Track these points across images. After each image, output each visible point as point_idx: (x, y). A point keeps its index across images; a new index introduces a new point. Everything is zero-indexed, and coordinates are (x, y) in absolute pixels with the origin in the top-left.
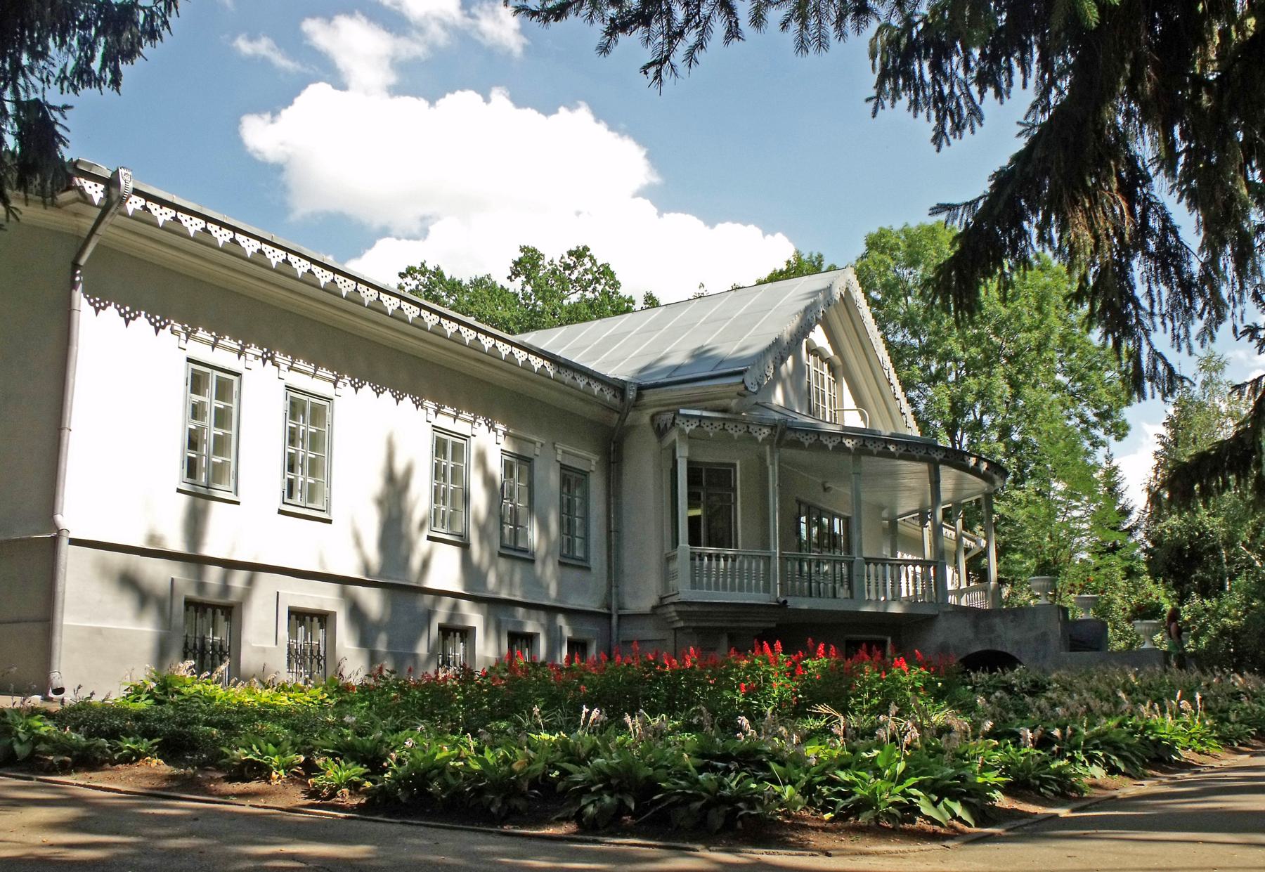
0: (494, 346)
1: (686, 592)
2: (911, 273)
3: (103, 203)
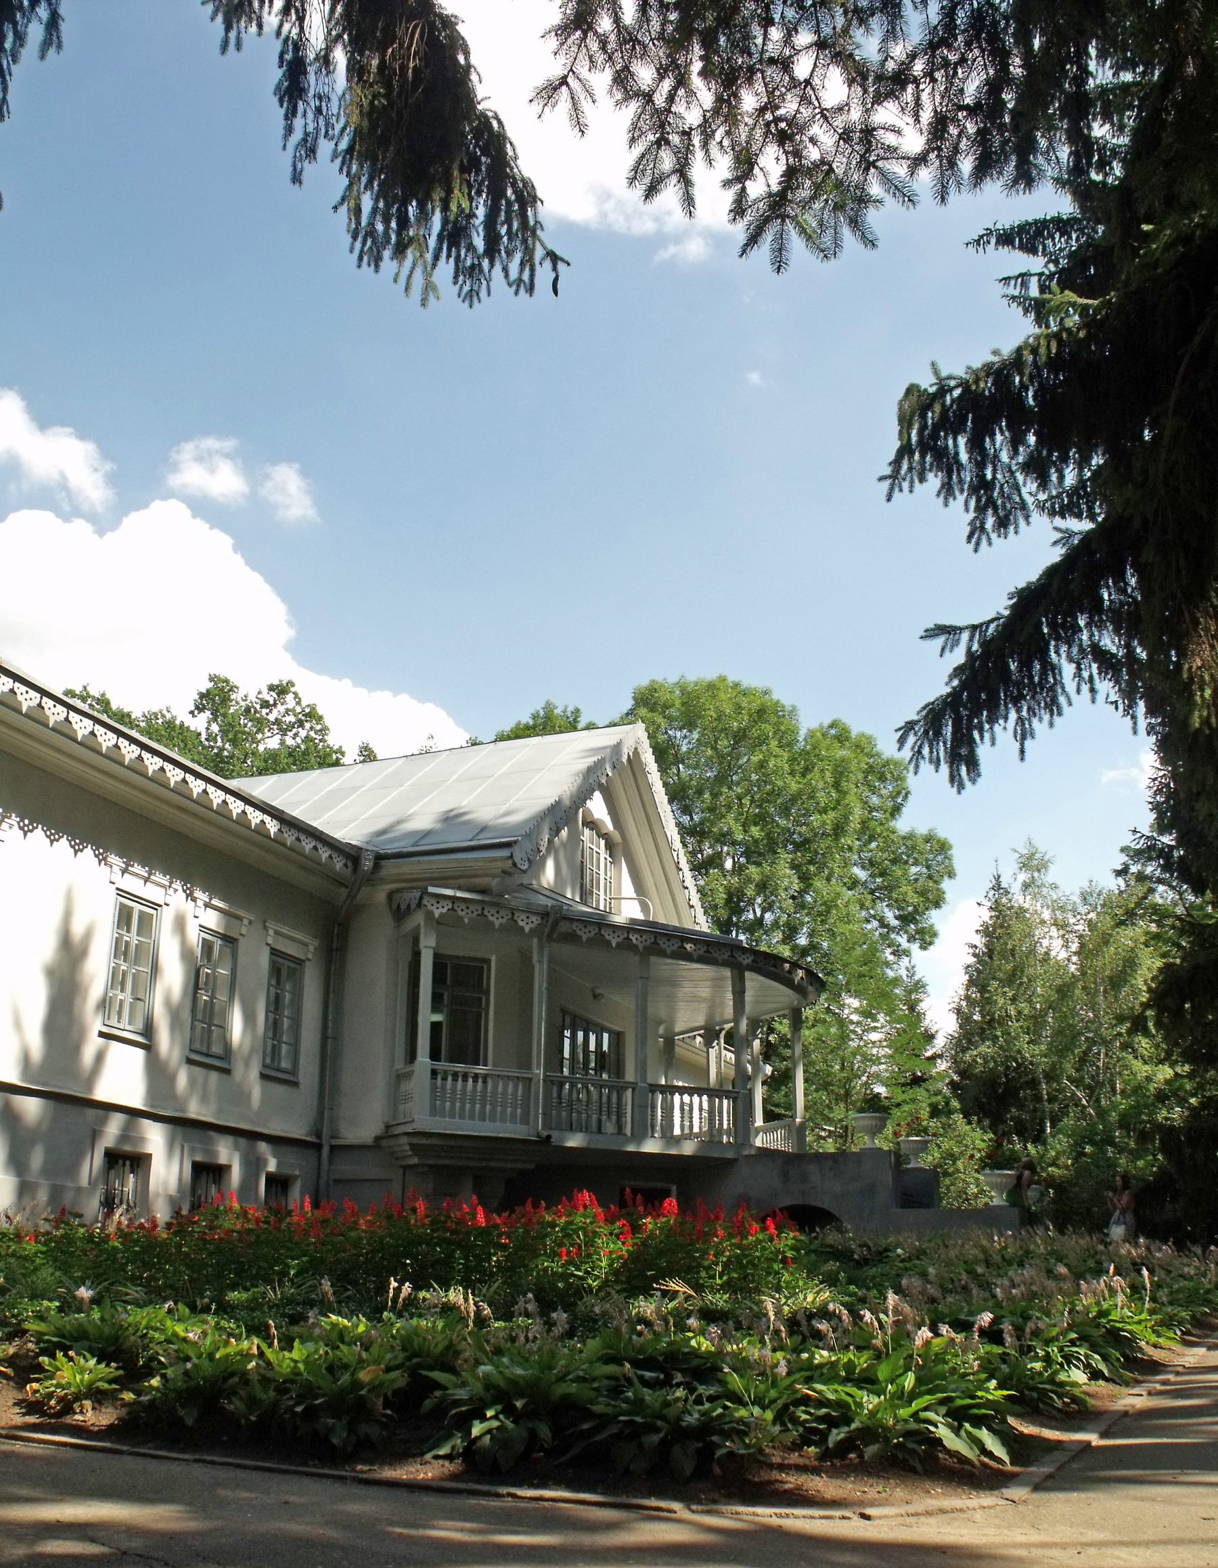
0: (205, 791)
1: (423, 1120)
2: (685, 737)
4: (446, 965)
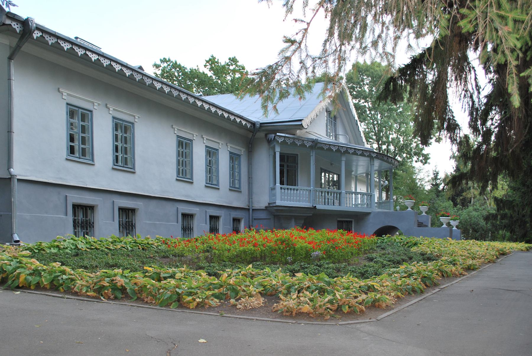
3: (22, 33)
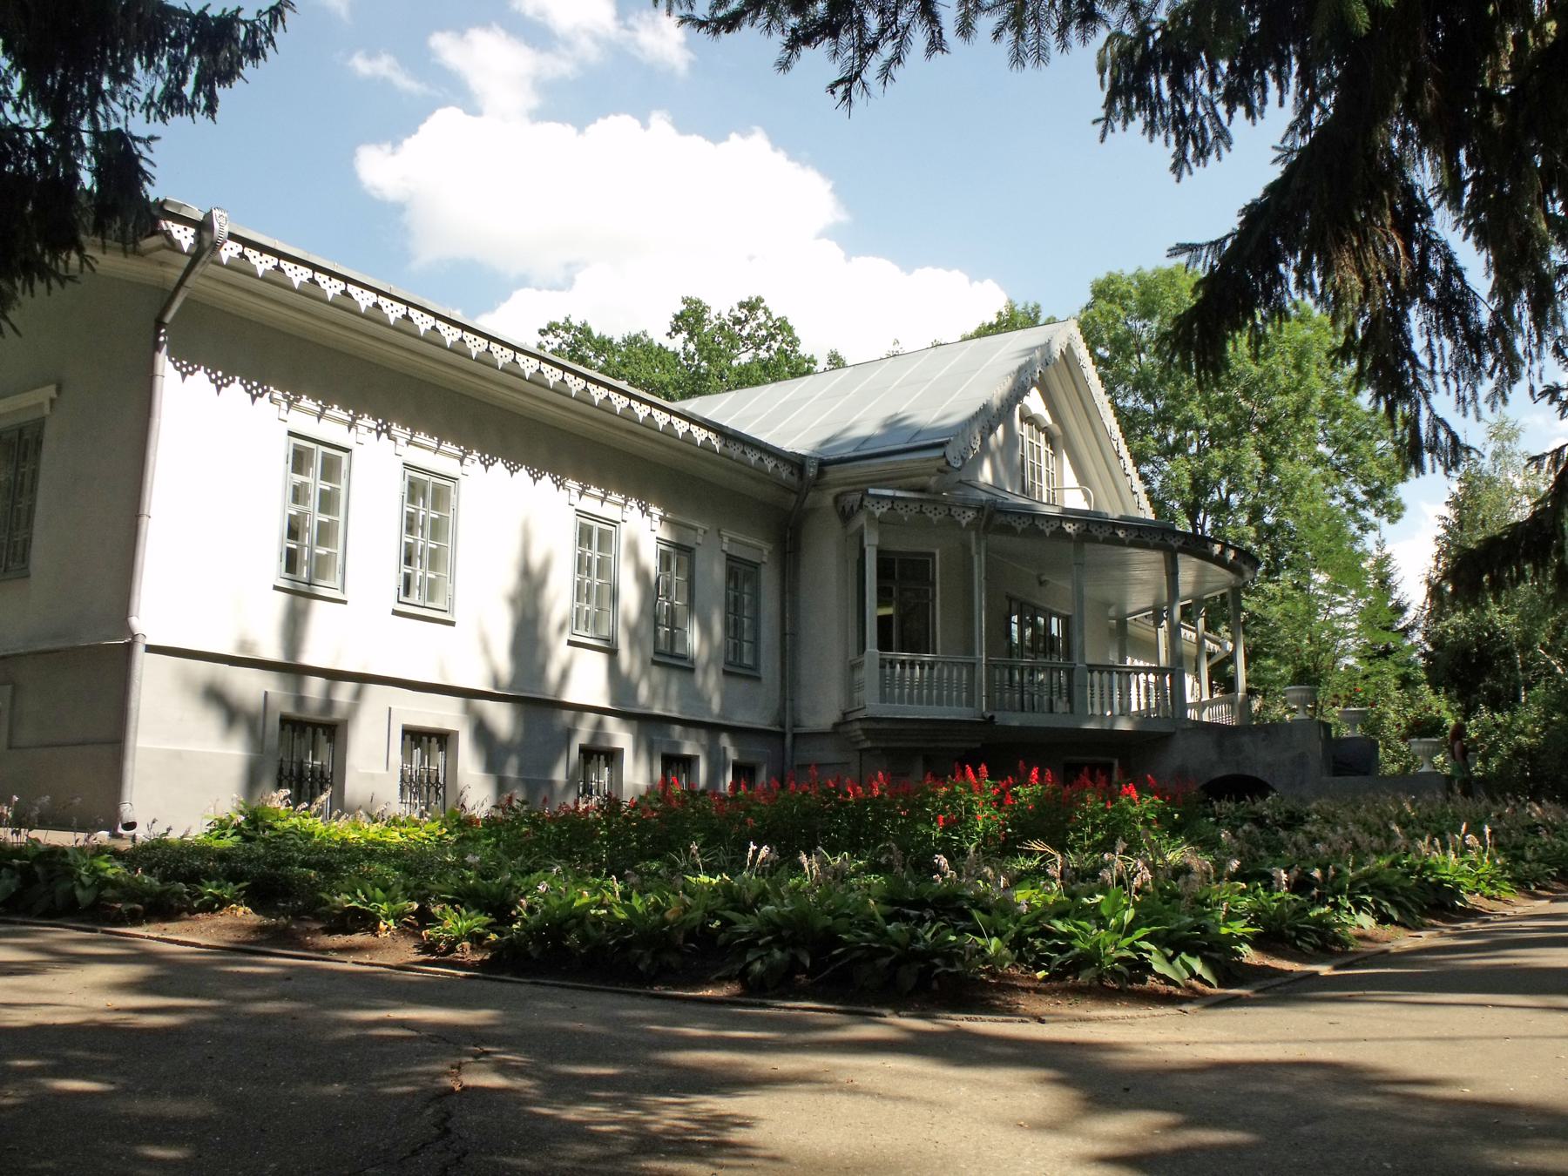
0: (650, 415)
1: (872, 704)
2: (1145, 326)
4: (893, 560)
